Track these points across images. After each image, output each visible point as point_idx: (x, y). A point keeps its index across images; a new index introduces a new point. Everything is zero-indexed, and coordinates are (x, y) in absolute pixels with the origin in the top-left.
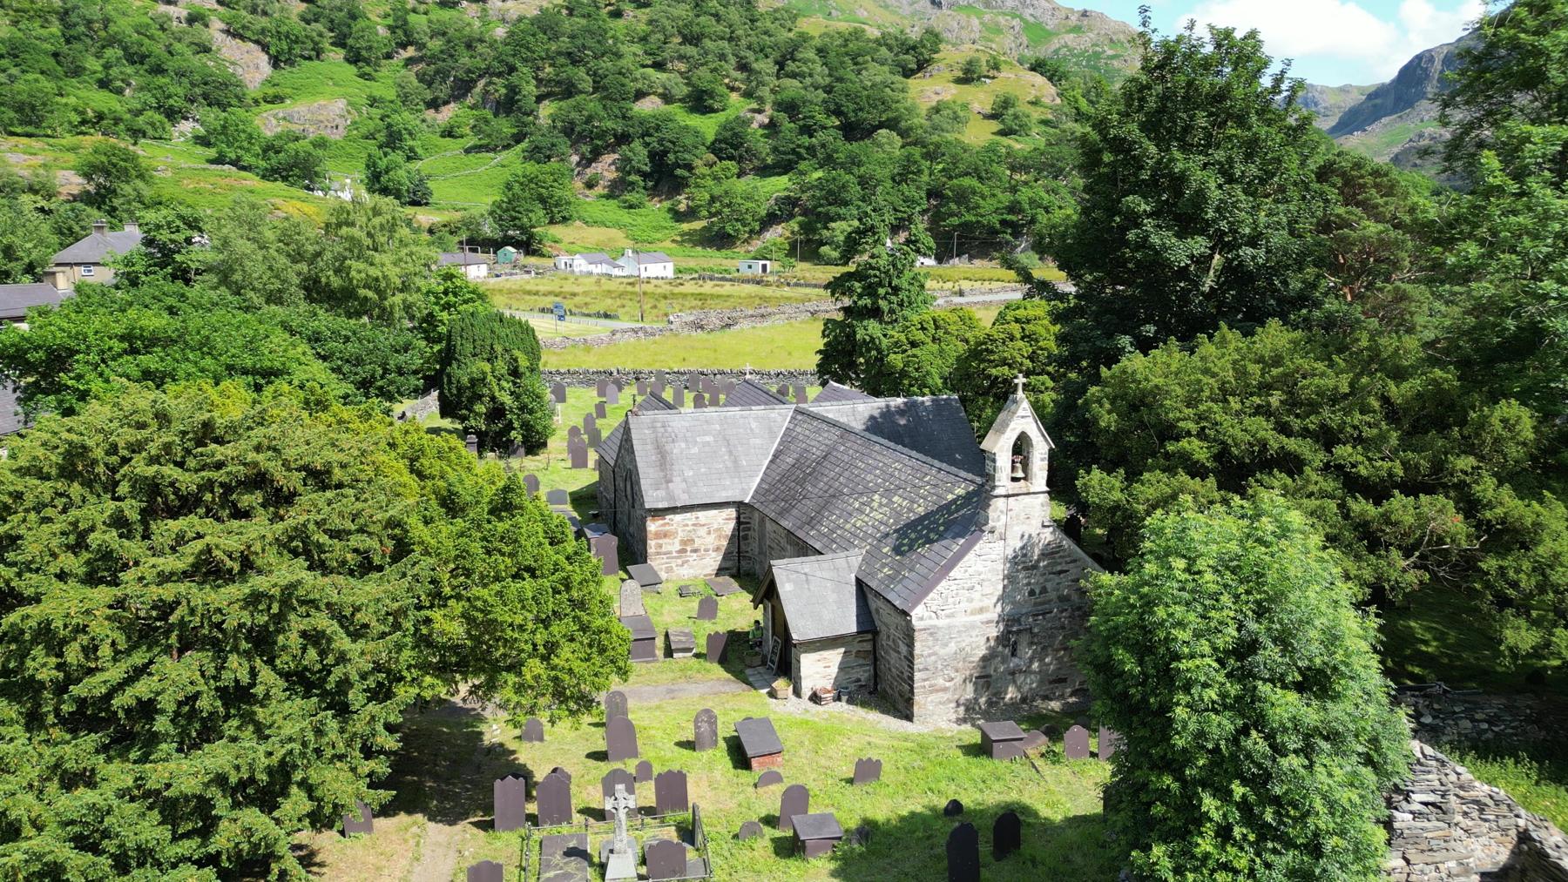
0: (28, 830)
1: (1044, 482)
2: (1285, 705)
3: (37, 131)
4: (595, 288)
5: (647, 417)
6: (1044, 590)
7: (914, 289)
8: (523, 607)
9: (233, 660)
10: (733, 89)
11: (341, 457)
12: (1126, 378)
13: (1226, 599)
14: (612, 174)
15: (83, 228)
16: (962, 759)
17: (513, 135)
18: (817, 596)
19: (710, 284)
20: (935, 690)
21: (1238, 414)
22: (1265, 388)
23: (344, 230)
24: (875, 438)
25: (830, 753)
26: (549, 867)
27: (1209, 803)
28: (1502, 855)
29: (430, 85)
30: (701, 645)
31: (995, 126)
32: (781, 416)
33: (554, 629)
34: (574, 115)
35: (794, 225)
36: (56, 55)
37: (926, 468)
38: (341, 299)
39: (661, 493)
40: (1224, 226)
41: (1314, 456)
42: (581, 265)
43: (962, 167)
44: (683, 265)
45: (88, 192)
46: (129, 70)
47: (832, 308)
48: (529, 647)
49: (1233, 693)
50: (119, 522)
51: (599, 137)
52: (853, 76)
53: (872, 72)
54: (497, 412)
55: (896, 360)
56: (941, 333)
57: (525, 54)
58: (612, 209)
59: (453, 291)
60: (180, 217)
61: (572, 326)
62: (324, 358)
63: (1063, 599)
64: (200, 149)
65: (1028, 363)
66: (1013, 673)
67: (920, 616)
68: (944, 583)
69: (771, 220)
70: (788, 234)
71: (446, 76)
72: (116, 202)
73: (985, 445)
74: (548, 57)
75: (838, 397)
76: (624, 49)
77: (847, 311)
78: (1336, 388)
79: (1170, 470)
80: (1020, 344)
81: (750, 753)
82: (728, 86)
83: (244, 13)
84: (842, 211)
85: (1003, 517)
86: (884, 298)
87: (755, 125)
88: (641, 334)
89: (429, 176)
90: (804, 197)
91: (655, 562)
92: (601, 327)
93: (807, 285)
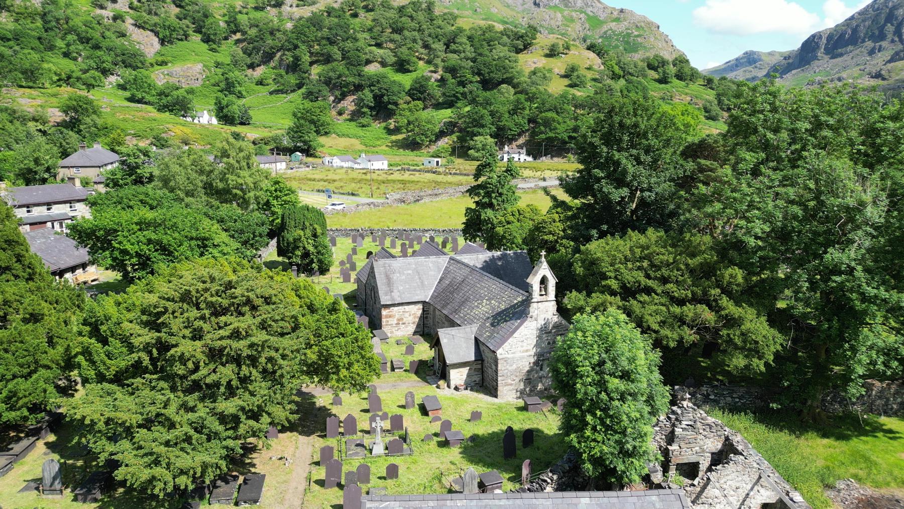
0: (178, 426)
2: (614, 383)
3: (35, 85)
4: (345, 176)
7: (510, 194)
9: (244, 367)
10: (420, 59)
11: (273, 292)
13: (595, 346)
14: (352, 107)
15: (67, 143)
16: (516, 412)
17: (297, 84)
18: (457, 344)
22: (642, 259)
26: (350, 450)
27: (589, 418)
28: (719, 446)
29: (249, 55)
30: (407, 366)
31: (567, 82)
32: (443, 261)
33: (352, 357)
34: (331, 74)
35: (454, 137)
36: (39, 38)
38: (224, 195)
39: (388, 297)
42: (337, 162)
45: (65, 121)
46: (81, 47)
54: (306, 254)
55: (500, 230)
57: (303, 38)
58: (352, 127)
62: (226, 230)
64: (121, 92)
65: (562, 233)
66: (541, 378)
67: (500, 353)
68: (511, 339)
69: (441, 134)
70: (451, 142)
71: (259, 50)
72: (82, 127)
73: (528, 281)
74: (317, 40)
76: (359, 36)
77: (477, 203)
79: (602, 292)
80: (558, 224)
81: (428, 409)
83: (144, 14)
84: (481, 130)
87: (433, 80)
89: (249, 108)
91: (385, 329)
92: (349, 201)
93: (461, 174)
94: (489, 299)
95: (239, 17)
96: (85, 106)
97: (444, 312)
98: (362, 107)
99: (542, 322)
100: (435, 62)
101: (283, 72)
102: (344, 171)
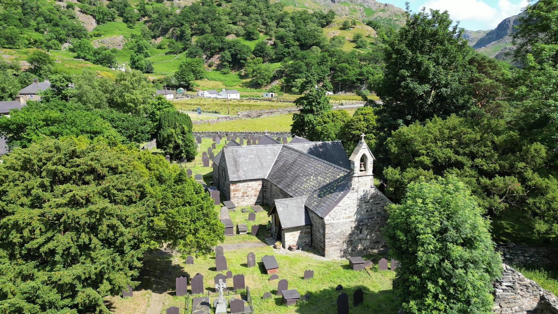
0: (10, 296)
1: (372, 171)
2: (457, 251)
3: (13, 47)
4: (212, 103)
5: (230, 148)
6: (371, 210)
7: (325, 103)
8: (186, 216)
9: (83, 235)
10: (261, 32)
11: (121, 163)
12: (401, 135)
13: (436, 213)
14: (218, 62)
16: (342, 270)
17: (183, 48)
18: (291, 212)
19: (253, 101)
20: (333, 246)
21: (440, 147)
22: (450, 138)
23: (123, 82)
24: (311, 156)
25: (295, 268)
26: (195, 309)
27: (430, 286)
28: (535, 304)
29: (153, 30)
30: (250, 230)
31: (354, 45)
32: (278, 148)
33: (197, 224)
34: (204, 41)
35: (283, 80)
36: (20, 20)
37: (329, 167)
38: (121, 106)
39: (235, 176)
40: (436, 80)
41: (468, 162)
42: (207, 94)
43: (342, 59)
44: (243, 94)
45: (31, 68)
46: (46, 25)
47: (296, 110)
48: (188, 230)
49: (439, 247)
50: (42, 186)
51: (213, 49)
52: (303, 27)
53: (310, 25)
54: (177, 147)
55: (319, 128)
56: (335, 118)
57: (187, 19)
58: (218, 74)
59: (161, 104)
60: (64, 77)
61: (204, 116)
62: (115, 128)
63: (378, 213)
64: (71, 53)
65: (366, 129)
66: (360, 240)
67: (327, 219)
68: (336, 208)
69: (274, 78)
70: (280, 83)
71: (159, 27)
72: (41, 72)
73: (350, 158)
74: (195, 20)
75: (298, 141)
76: (222, 17)
77: (301, 111)
78: (476, 138)
79: (416, 167)
80: (363, 122)
81: (267, 268)
82: (259, 31)
83: (87, 5)
84: (300, 75)
85: (357, 184)
86: (315, 106)
87: (269, 45)
88: (228, 119)
89: (153, 63)
90: (286, 70)
91: (233, 200)
92: (214, 117)
93: (287, 102)
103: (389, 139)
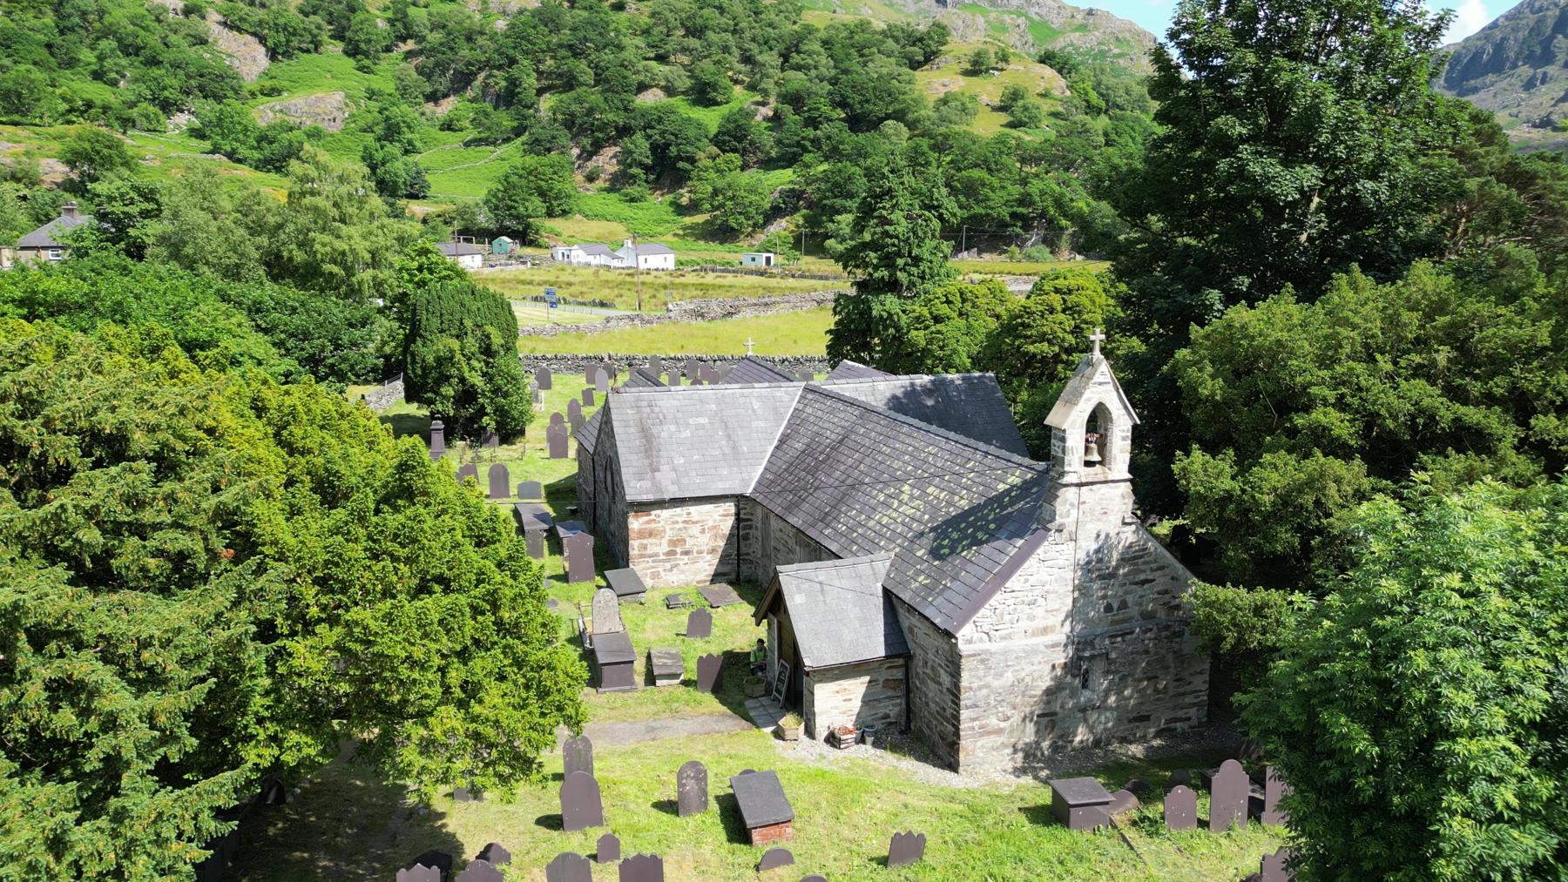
1: (1126, 467)
3: (24, 120)
5: (631, 395)
6: (1123, 605)
8: (426, 635)
10: (736, 82)
11: (152, 417)
12: (1231, 335)
14: (613, 167)
17: (514, 129)
18: (835, 612)
19: (712, 275)
20: (986, 732)
21: (1390, 377)
23: (308, 200)
24: (902, 417)
25: (856, 820)
29: (429, 78)
31: (1004, 118)
32: (789, 395)
34: (575, 107)
35: (798, 218)
36: (49, 46)
37: (968, 452)
38: (308, 275)
39: (647, 484)
40: (1341, 151)
41: (1506, 432)
42: (579, 255)
43: (971, 158)
44: (684, 258)
45: (72, 180)
46: (124, 61)
48: (437, 690)
49: (1545, 794)
51: (601, 129)
52: (859, 69)
53: (878, 63)
54: (467, 395)
55: (918, 337)
56: (968, 306)
57: (526, 46)
58: (613, 204)
59: (427, 268)
60: (134, 188)
61: (563, 314)
62: (266, 331)
63: (1147, 616)
64: (195, 142)
66: (1083, 710)
67: (968, 638)
69: (775, 213)
70: (792, 227)
71: (448, 67)
73: (1050, 420)
74: (550, 50)
76: (626, 41)
78: (1533, 338)
80: (1062, 317)
81: (749, 822)
82: (732, 79)
85: (1074, 513)
86: (903, 269)
87: (759, 118)
90: (809, 190)
91: (639, 566)
93: (813, 277)
94: (921, 483)
95: (412, 11)
96: (105, 151)
97: (792, 520)
98: (630, 166)
99: (1089, 545)
100: (763, 85)
101: (488, 107)
102: (591, 270)
103: (1182, 354)
